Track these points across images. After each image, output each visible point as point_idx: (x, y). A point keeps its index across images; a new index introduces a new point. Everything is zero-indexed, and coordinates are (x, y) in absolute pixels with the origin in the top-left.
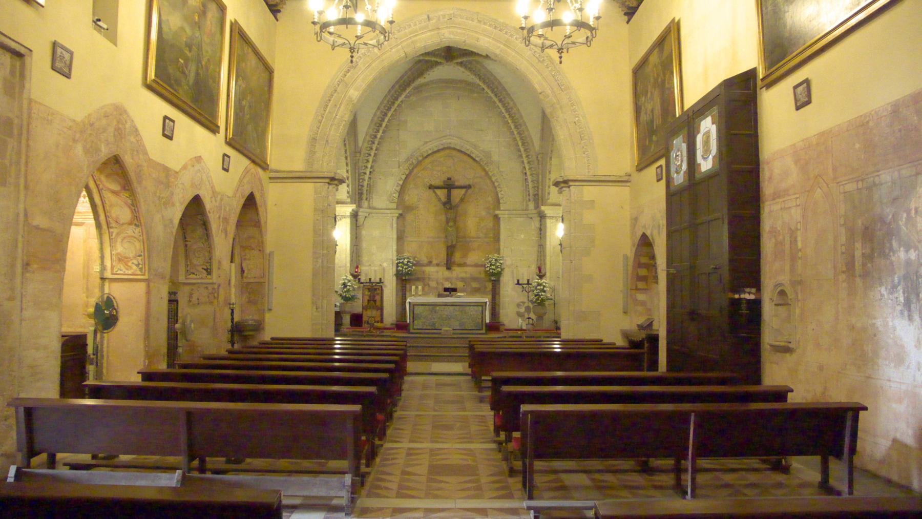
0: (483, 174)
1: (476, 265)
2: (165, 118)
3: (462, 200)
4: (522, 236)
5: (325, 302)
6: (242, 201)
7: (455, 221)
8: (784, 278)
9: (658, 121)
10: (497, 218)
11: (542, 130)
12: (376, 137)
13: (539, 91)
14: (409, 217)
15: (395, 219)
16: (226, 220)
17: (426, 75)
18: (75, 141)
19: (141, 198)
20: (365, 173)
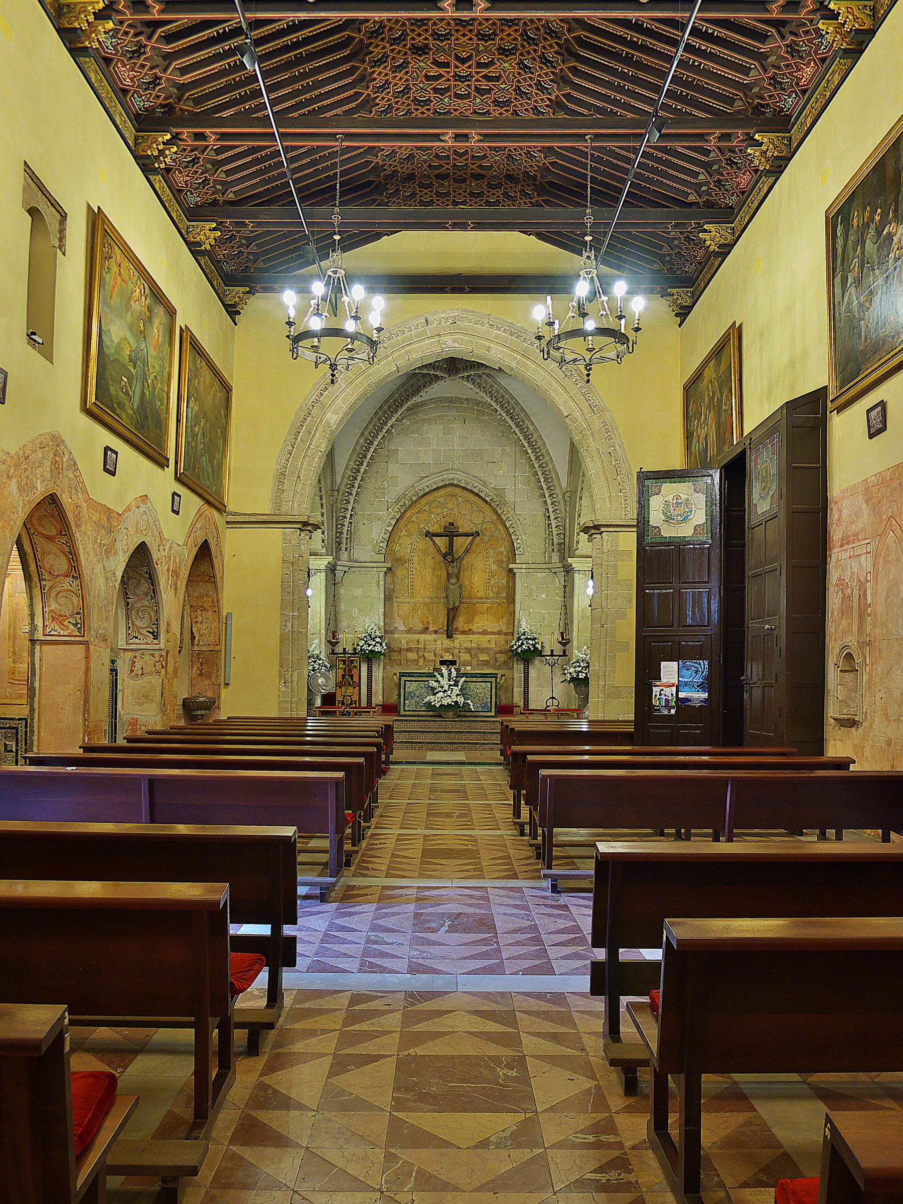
2: (107, 449)
3: (467, 551)
4: (544, 596)
5: (295, 674)
6: (195, 550)
8: (852, 640)
11: (571, 461)
13: (566, 414)
14: (400, 572)
15: (382, 575)
16: (176, 574)
18: (9, 477)
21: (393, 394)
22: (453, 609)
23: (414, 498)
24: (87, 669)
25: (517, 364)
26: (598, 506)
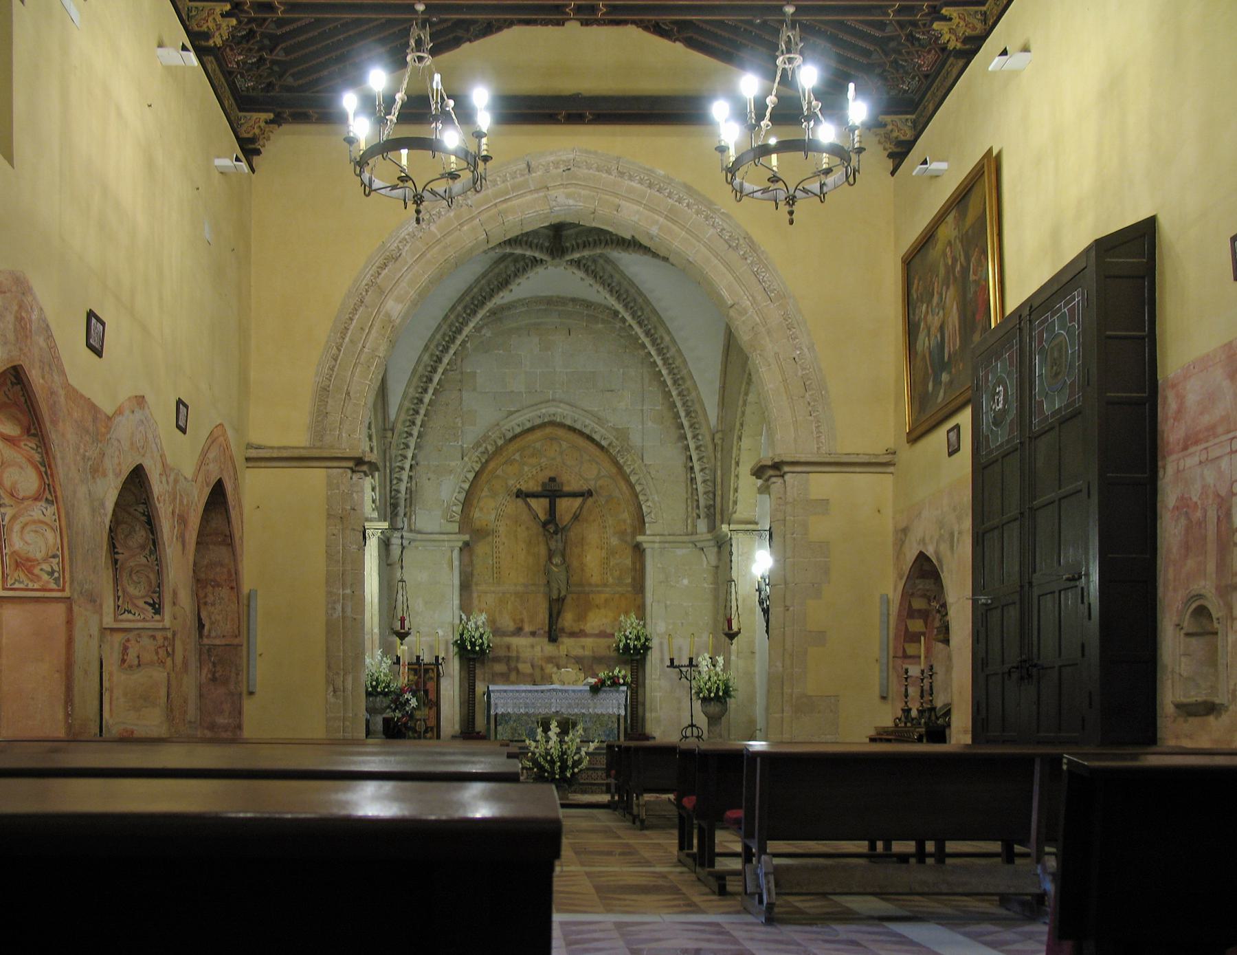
0: (614, 470)
1: (602, 634)
3: (576, 517)
4: (686, 582)
6: (207, 491)
7: (563, 556)
8: (1206, 586)
9: (953, 344)
10: (638, 550)
12: (421, 401)
13: (730, 303)
14: (481, 549)
15: (456, 553)
16: (183, 520)
17: (513, 287)
19: (56, 450)
20: (402, 468)
21: (470, 289)
22: (558, 600)
23: (500, 442)
24: (70, 641)
25: (660, 229)
26: (778, 436)
